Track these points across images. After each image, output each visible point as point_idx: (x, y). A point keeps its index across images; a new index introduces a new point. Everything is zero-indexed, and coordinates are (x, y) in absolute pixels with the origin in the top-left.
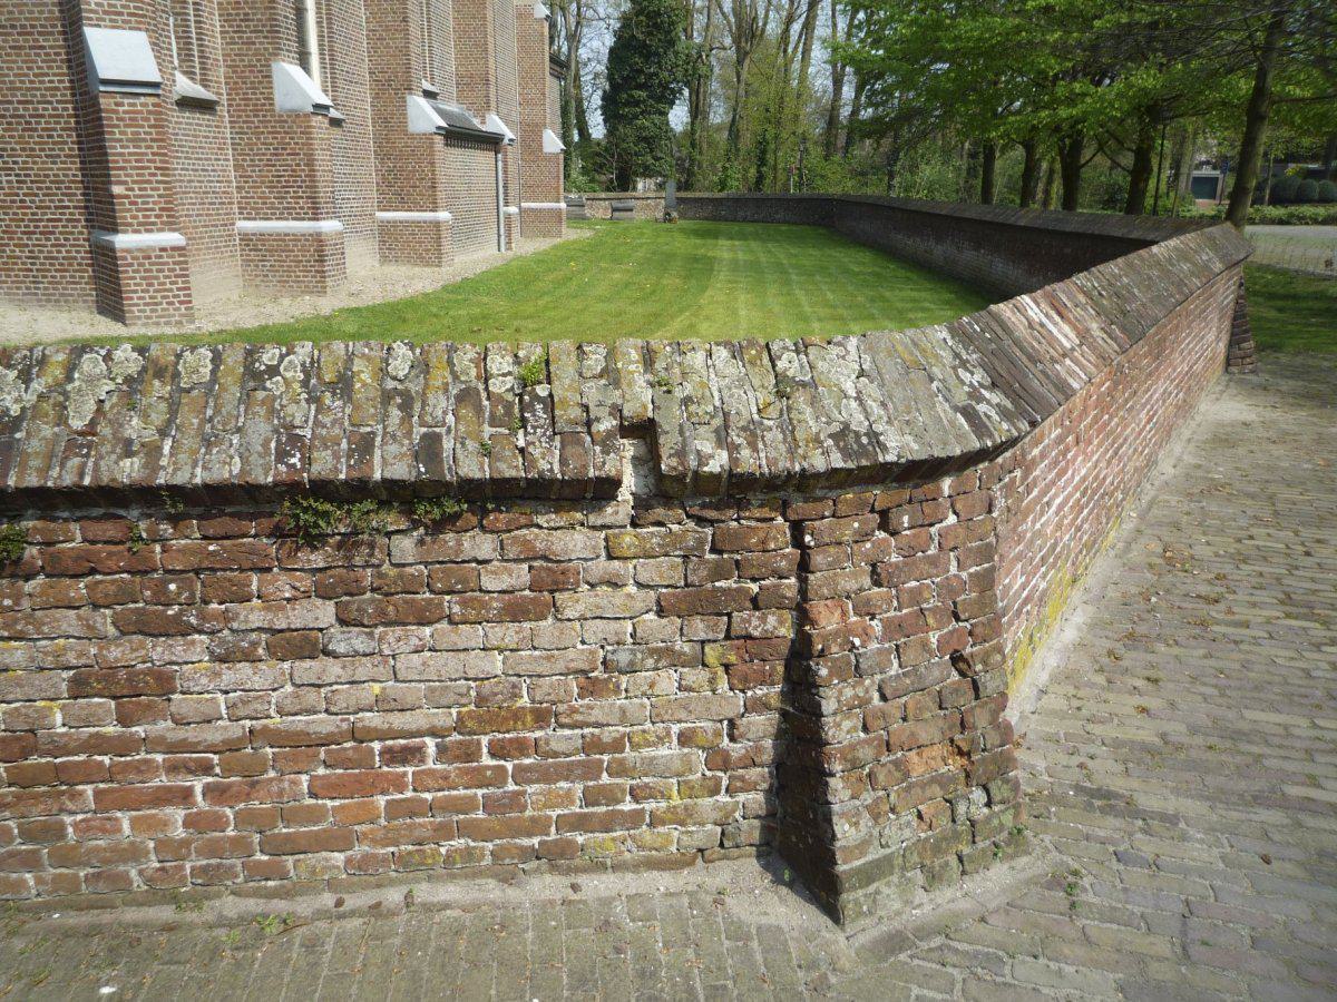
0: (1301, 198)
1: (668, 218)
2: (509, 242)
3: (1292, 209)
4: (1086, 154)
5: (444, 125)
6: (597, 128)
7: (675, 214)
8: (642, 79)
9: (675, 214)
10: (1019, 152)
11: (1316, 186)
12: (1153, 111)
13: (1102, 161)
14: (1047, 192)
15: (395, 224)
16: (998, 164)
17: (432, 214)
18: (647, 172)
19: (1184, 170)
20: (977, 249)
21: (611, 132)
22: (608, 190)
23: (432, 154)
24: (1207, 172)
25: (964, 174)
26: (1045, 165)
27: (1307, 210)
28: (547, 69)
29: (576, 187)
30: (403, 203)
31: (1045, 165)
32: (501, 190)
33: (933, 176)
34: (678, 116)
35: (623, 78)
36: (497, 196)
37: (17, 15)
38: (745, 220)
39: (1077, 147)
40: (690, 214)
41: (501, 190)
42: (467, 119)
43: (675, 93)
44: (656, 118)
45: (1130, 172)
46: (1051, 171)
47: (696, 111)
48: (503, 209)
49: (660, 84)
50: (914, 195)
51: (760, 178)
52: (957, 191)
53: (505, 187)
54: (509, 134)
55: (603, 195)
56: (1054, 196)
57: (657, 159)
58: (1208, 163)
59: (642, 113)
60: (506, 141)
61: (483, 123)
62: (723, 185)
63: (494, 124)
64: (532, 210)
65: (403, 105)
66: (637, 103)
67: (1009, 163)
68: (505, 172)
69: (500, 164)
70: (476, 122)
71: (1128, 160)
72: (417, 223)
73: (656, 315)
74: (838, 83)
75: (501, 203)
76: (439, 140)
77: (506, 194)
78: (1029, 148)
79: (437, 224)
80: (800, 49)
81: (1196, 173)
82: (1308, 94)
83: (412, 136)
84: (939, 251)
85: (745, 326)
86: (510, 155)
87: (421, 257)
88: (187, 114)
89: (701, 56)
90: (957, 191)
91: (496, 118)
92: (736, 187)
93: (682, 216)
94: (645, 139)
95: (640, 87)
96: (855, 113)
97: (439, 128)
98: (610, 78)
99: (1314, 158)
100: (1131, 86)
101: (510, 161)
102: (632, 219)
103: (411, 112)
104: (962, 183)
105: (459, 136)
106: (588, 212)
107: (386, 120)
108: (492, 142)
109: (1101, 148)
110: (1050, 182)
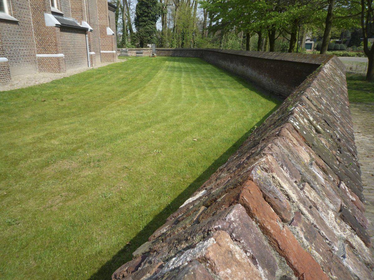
0: (335, 49)
1: (153, 56)
2: (92, 64)
3: (334, 52)
4: (276, 36)
5: (59, 23)
6: (135, 30)
7: (155, 55)
8: (146, 14)
9: (155, 55)
10: (257, 36)
11: (339, 46)
12: (296, 22)
13: (281, 38)
14: (265, 48)
15: (43, 58)
16: (251, 39)
17: (56, 55)
18: (149, 42)
19: (303, 41)
20: (243, 65)
21: (138, 30)
22: (137, 47)
23: (55, 34)
24: (309, 42)
25: (242, 43)
26: (265, 40)
27: (337, 52)
28: (107, 8)
29: (128, 47)
30: (46, 51)
31: (265, 40)
32: (88, 47)
33: (233, 42)
34: (159, 26)
35: (140, 13)
36: (87, 49)
37: (35, 12)
38: (177, 56)
39: (274, 33)
40: (161, 54)
41: (88, 47)
42: (75, 23)
43: (157, 19)
44: (151, 26)
45: (290, 41)
46: (266, 41)
47: (163, 23)
48: (89, 53)
49: (152, 16)
50: (227, 48)
51: (183, 44)
52: (240, 47)
53: (90, 46)
54: (90, 28)
55: (134, 49)
56: (267, 49)
57: (151, 38)
58: (309, 39)
59: (146, 24)
60: (89, 30)
61: (81, 24)
62: (172, 46)
63: (85, 24)
64: (104, 53)
65: (43, 16)
66: (145, 21)
67: (254, 38)
68: (89, 40)
69: (87, 38)
70: (79, 24)
71: (289, 36)
72: (51, 58)
73: (125, 91)
74: (205, 16)
75: (88, 51)
76: (58, 30)
77: (90, 48)
78: (260, 34)
79: (58, 58)
80: (194, 5)
81: (306, 42)
82: (344, 16)
83: (47, 28)
84: (231, 66)
85: (39, 136)
86: (91, 35)
87: (53, 70)
88: (5, 24)
89: (163, 7)
90: (240, 47)
91: (109, 28)
92: (175, 47)
93: (158, 55)
94: (148, 32)
95: (145, 16)
96: (210, 24)
97: (56, 25)
98: (137, 14)
99: (337, 38)
100: (290, 13)
101: (91, 37)
102: (142, 56)
103: (46, 19)
104: (241, 45)
105: (65, 28)
106: (129, 54)
107: (37, 22)
108: (84, 31)
109: (281, 33)
110: (266, 44)
